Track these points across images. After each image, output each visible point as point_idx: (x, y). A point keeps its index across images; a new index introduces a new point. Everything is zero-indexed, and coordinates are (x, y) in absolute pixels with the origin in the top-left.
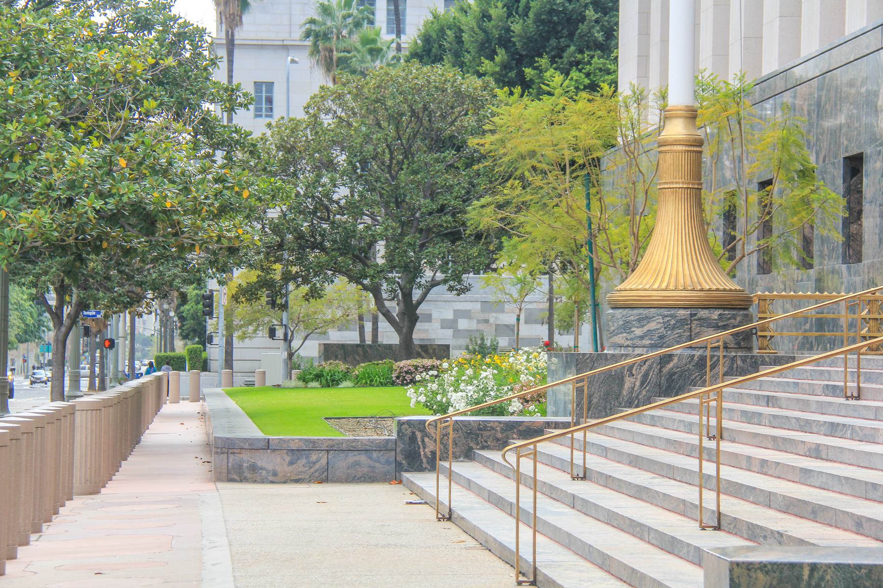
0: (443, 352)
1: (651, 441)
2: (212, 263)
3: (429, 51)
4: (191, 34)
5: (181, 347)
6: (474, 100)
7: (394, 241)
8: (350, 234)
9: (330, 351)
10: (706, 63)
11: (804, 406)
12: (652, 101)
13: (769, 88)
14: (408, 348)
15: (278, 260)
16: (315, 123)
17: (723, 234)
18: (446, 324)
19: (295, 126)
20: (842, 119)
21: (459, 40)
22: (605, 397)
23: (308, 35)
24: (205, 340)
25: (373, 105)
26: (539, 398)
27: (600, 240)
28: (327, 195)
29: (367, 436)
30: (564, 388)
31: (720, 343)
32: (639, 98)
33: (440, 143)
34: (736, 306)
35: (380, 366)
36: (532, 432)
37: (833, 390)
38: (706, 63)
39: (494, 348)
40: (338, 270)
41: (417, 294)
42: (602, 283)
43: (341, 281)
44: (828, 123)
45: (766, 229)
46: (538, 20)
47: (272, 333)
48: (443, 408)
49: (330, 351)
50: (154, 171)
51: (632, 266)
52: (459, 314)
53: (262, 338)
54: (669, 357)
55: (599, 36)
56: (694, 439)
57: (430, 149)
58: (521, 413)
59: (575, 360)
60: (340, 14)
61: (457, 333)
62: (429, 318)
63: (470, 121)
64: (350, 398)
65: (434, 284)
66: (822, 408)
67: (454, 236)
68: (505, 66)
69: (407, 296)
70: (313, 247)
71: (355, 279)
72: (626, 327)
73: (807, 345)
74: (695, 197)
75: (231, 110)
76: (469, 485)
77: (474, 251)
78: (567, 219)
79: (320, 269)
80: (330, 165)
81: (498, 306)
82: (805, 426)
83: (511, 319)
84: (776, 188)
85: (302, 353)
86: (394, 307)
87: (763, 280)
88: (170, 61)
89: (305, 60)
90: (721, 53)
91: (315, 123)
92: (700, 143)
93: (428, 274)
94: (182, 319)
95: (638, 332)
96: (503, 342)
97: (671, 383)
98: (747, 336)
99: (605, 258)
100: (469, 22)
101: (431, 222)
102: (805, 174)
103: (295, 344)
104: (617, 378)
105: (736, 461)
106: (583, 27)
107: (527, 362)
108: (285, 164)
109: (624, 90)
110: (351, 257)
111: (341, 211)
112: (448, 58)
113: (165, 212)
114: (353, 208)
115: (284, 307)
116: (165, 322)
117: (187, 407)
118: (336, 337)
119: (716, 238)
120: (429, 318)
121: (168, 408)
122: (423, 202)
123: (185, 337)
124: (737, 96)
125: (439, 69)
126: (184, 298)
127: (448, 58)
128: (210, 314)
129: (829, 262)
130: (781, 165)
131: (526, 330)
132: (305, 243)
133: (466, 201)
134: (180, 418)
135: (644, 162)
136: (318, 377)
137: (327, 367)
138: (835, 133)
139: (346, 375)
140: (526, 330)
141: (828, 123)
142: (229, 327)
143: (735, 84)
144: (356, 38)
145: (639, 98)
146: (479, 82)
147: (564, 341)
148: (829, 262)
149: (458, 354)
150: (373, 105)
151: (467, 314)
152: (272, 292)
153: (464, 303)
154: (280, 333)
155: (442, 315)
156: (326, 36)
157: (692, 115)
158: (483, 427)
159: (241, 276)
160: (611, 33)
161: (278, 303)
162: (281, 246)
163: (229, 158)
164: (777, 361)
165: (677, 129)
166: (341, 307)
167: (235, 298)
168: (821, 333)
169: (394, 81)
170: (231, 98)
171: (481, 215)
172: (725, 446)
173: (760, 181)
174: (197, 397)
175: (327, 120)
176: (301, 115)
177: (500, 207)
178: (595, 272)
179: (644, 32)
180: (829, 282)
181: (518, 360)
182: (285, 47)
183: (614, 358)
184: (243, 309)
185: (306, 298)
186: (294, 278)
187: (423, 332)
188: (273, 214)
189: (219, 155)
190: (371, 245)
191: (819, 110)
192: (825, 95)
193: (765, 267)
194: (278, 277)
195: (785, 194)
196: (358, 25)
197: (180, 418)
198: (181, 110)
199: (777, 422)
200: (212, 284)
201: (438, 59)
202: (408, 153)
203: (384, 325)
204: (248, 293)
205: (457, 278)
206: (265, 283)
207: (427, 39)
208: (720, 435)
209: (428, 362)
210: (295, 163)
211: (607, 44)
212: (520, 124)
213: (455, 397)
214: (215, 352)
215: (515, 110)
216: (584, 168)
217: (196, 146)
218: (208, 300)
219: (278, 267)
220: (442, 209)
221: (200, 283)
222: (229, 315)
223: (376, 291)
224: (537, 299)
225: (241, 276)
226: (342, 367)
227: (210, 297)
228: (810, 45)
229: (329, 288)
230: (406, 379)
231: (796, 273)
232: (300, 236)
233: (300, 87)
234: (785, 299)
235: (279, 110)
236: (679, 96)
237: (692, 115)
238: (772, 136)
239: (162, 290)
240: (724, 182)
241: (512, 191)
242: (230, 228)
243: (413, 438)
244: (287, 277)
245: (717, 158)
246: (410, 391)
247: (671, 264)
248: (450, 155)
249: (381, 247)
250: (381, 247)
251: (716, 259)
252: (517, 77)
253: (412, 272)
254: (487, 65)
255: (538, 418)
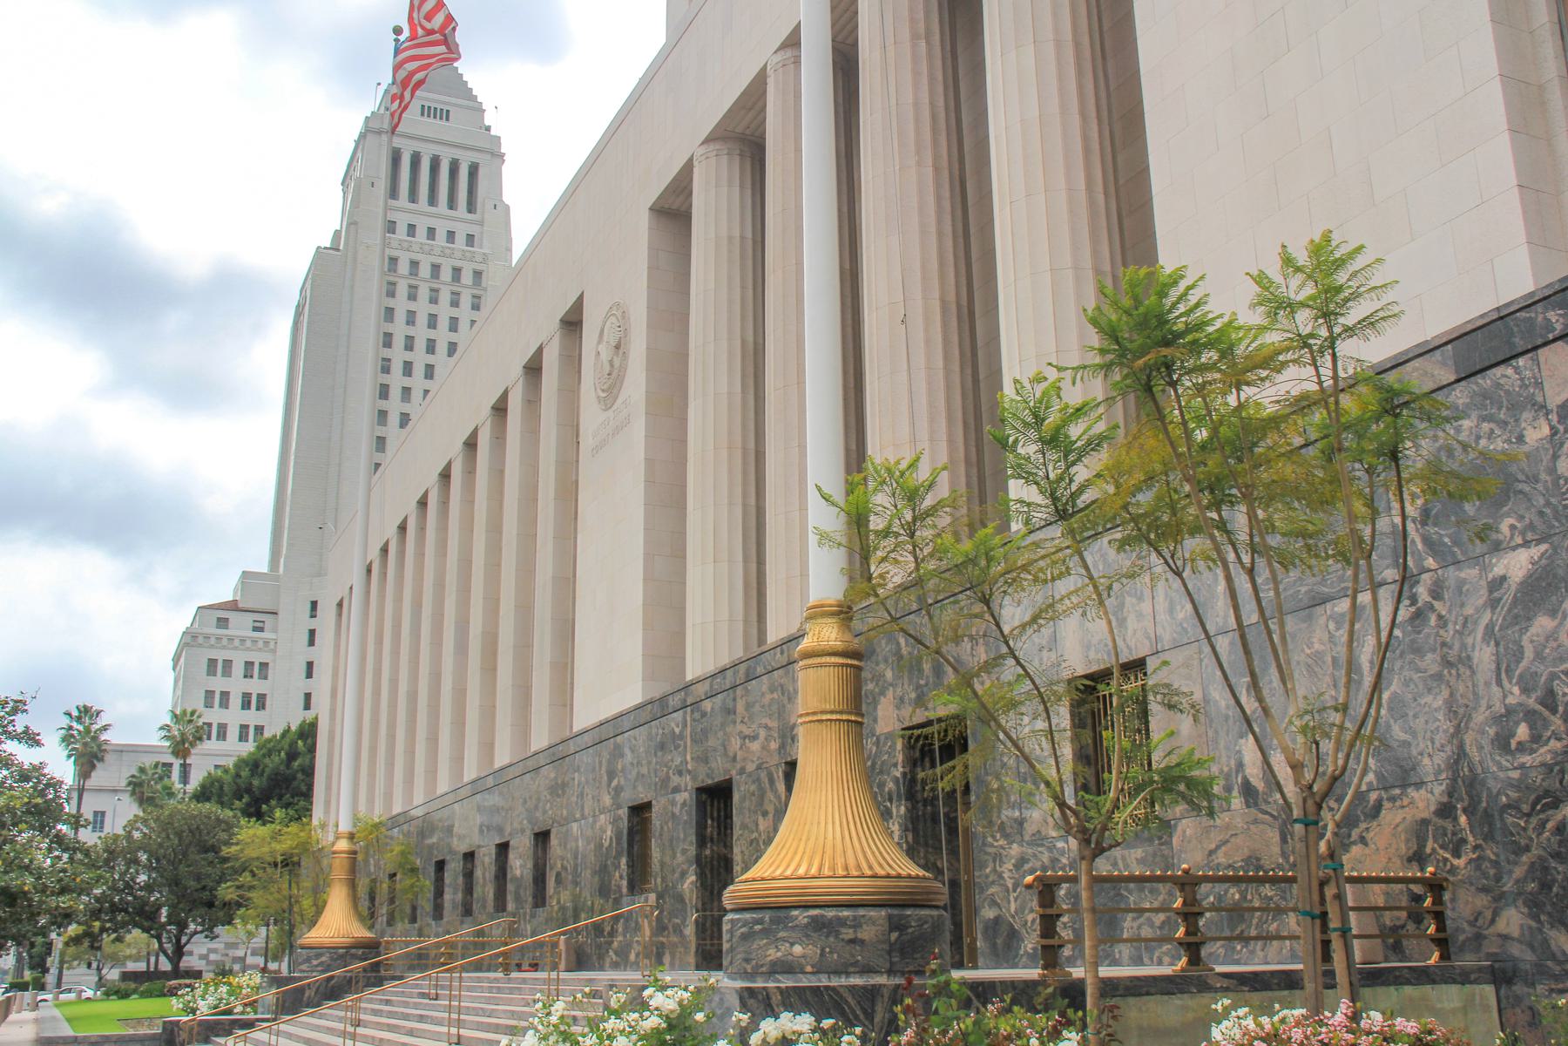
0: (198, 975)
1: (318, 1028)
2: (53, 924)
3: (203, 795)
4: (55, 784)
5: (28, 975)
6: (227, 823)
7: (173, 907)
8: (146, 903)
9: (126, 976)
10: (362, 808)
11: (406, 1005)
12: (331, 829)
13: (395, 821)
14: (177, 973)
15: (98, 919)
16: (129, 836)
17: (367, 906)
18: (202, 957)
19: (116, 837)
20: (434, 840)
21: (221, 788)
22: (293, 1002)
23: (129, 784)
24: (46, 971)
25: (166, 826)
26: (253, 1004)
27: (296, 909)
28: (133, 879)
29: (142, 1031)
30: (270, 995)
31: (361, 970)
32: (323, 826)
33: (206, 849)
34: (371, 947)
35: (158, 984)
36: (249, 1025)
37: (423, 995)
38: (362, 808)
39: (231, 972)
40: (136, 925)
41: (184, 939)
42: (297, 932)
43: (137, 932)
44: (429, 841)
45: (392, 901)
46: (269, 778)
47: (89, 966)
48: (194, 1011)
49: (126, 976)
50: (20, 867)
51: (313, 923)
52: (211, 951)
53: (83, 969)
54: (332, 977)
55: (304, 788)
56: (341, 1026)
57: (199, 852)
58: (242, 1013)
59: (277, 980)
60: (150, 772)
61: (209, 962)
62: (191, 953)
63: (224, 836)
64: (137, 1006)
65: (196, 933)
66: (416, 1006)
67: (210, 905)
68: (248, 805)
69: (178, 940)
70: (121, 911)
71: (146, 930)
72: (308, 960)
73: (412, 968)
74: (352, 885)
75: (76, 830)
76: (290, 1036)
77: (221, 914)
78: (276, 896)
79: (124, 925)
80: (136, 861)
81: (234, 946)
82: (406, 1017)
83: (240, 953)
84: (398, 877)
85: (108, 977)
86: (169, 947)
87: (389, 930)
88: (39, 800)
89: (126, 798)
90: (371, 801)
91: (129, 836)
92: (355, 853)
93: (192, 927)
94: (31, 957)
95: (315, 962)
96: (236, 967)
97: (333, 992)
98: (378, 964)
99: (298, 919)
100: (228, 778)
101: (196, 895)
102: (414, 870)
103: (104, 972)
104: (301, 990)
105: (469, 1011)
106: (295, 784)
107: (249, 980)
108: (107, 861)
109: (315, 822)
110: (145, 917)
111: (141, 889)
112: (214, 798)
113: (25, 893)
114: (149, 888)
115: (99, 948)
116: (19, 959)
117: (28, 1015)
118: (132, 966)
119: (364, 904)
120: (191, 953)
121: (13, 1017)
122: (192, 884)
123: (32, 968)
124: (376, 826)
125: (208, 805)
126: (32, 945)
127: (214, 798)
128: (49, 954)
129: (426, 919)
130: (401, 866)
131: (250, 960)
132: (114, 909)
133: (219, 883)
134: (21, 1023)
135: (325, 862)
136: (116, 993)
137: (123, 986)
138: (431, 847)
139: (135, 991)
140: (250, 960)
141: (429, 841)
142: (62, 962)
143: (377, 820)
144: (159, 787)
145: (323, 826)
146: (231, 814)
147: (273, 966)
148: (426, 919)
149: (208, 976)
150: (166, 826)
151: (215, 951)
152: (90, 940)
153: (213, 945)
154: (94, 965)
155: (199, 951)
156: (140, 784)
157: (351, 837)
158: (217, 1022)
159: (73, 929)
160: (310, 787)
161: (95, 947)
162: (100, 911)
163: (71, 858)
164: (394, 978)
165: (343, 845)
166: (137, 948)
167: (67, 944)
168: (420, 961)
169: (179, 811)
170: (76, 822)
171: (226, 892)
172: (360, 1030)
173: (537, 830)
174: (35, 1006)
175: (137, 835)
176: (121, 832)
177: (238, 887)
178: (292, 926)
179: (328, 788)
180: (426, 931)
181: (244, 980)
182: (115, 791)
183: (301, 979)
184: (72, 950)
185: (113, 941)
186: (107, 930)
187: (187, 962)
188: (97, 891)
189: (66, 856)
190: (159, 908)
191: (422, 834)
192: (426, 827)
193: (391, 922)
194: (96, 930)
195: (403, 882)
196: (161, 778)
197: (21, 1023)
198: (43, 829)
199: (391, 1015)
200: (53, 936)
201: (208, 799)
202: (185, 854)
203: (162, 958)
204: (76, 940)
205: (210, 929)
206: (87, 934)
207: (203, 786)
208: (358, 1023)
209: (187, 981)
210: (114, 860)
211: (308, 795)
212: (253, 839)
213: (201, 1003)
214: (50, 979)
215: (251, 832)
216: (289, 864)
217: (50, 850)
218: (49, 946)
219: (97, 924)
220: (204, 888)
221: (45, 935)
222: (62, 954)
223: (159, 938)
224: (259, 941)
225: (73, 929)
226: (133, 986)
227: (51, 944)
228: (419, 798)
229: (128, 938)
230: (172, 992)
231: (408, 926)
232: (113, 904)
233: (122, 814)
234: (401, 942)
235: (107, 829)
236: (345, 826)
237: (351, 837)
238: (397, 849)
239: (19, 940)
240: (369, 874)
241: (246, 878)
242: (64, 902)
243: (172, 1031)
244: (103, 930)
245: (366, 861)
246: (174, 1000)
247: (336, 923)
248: (211, 855)
249: (164, 911)
250: (164, 911)
251: (361, 919)
252: (256, 812)
253: (182, 926)
254: (237, 803)
255: (252, 1016)
